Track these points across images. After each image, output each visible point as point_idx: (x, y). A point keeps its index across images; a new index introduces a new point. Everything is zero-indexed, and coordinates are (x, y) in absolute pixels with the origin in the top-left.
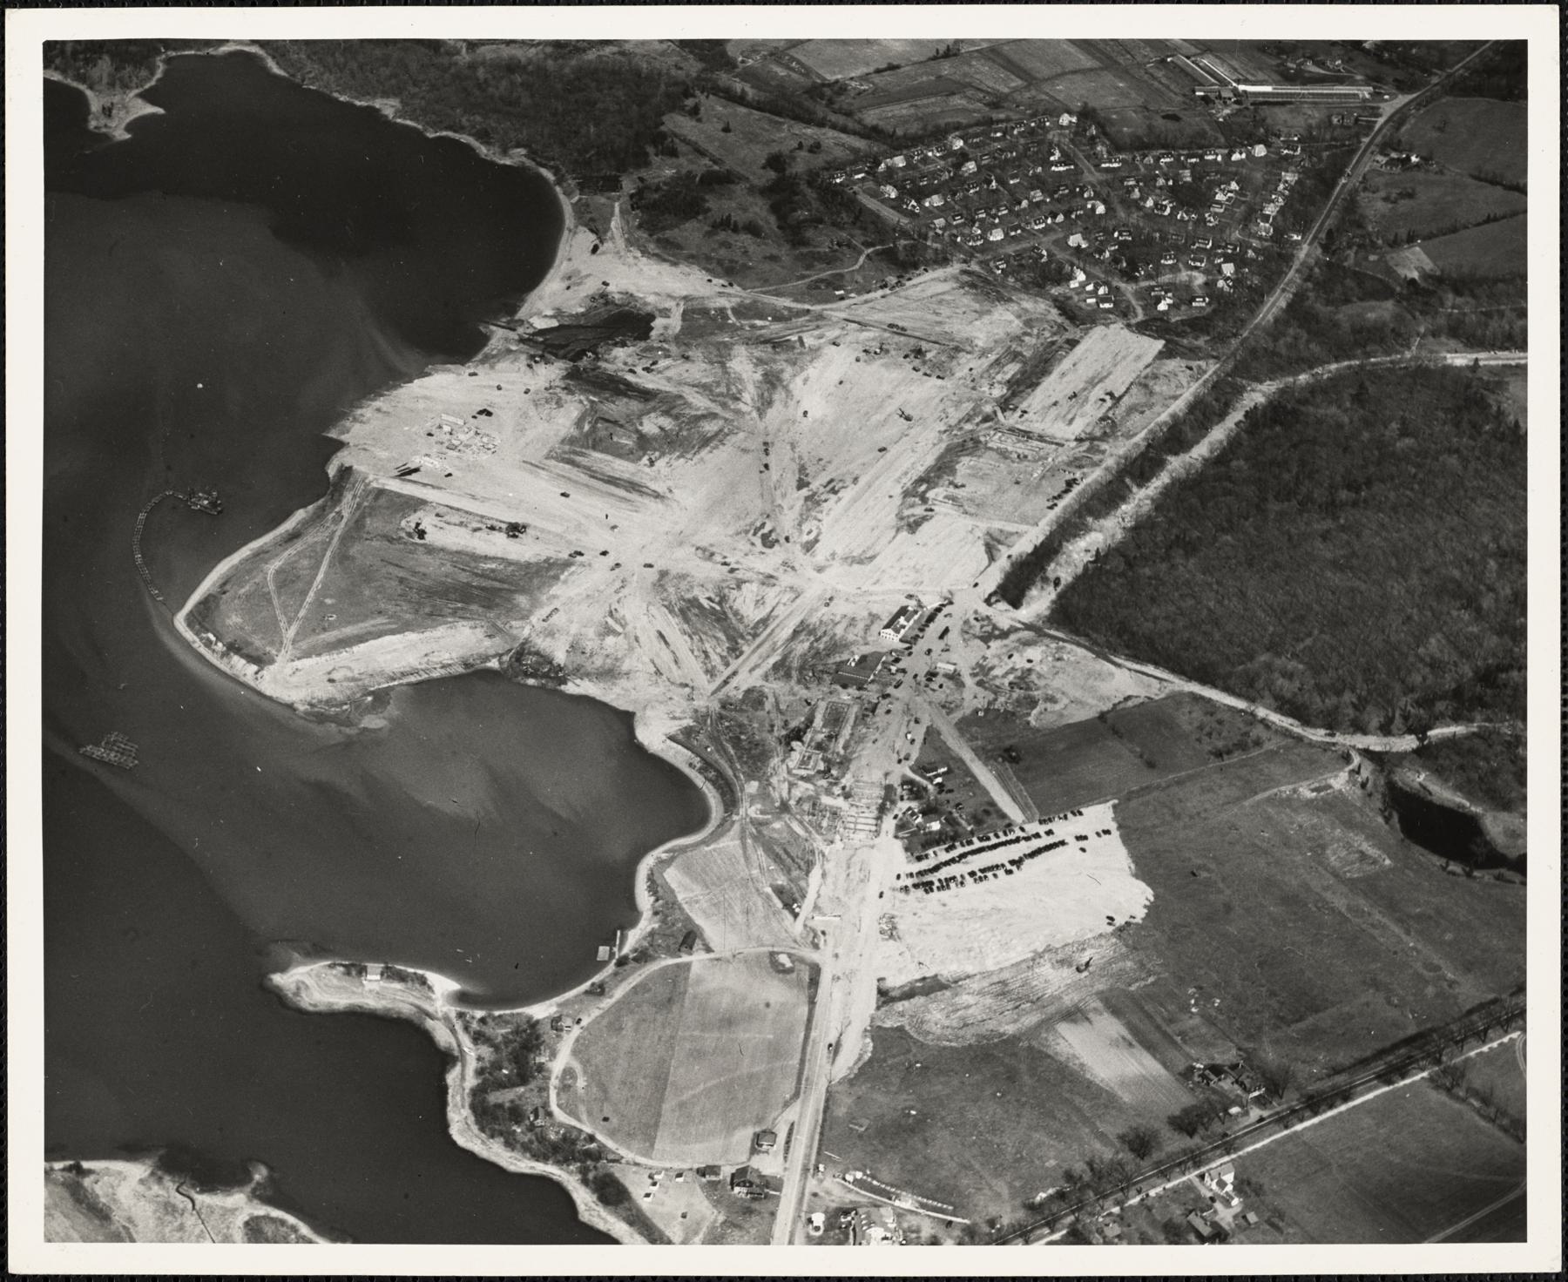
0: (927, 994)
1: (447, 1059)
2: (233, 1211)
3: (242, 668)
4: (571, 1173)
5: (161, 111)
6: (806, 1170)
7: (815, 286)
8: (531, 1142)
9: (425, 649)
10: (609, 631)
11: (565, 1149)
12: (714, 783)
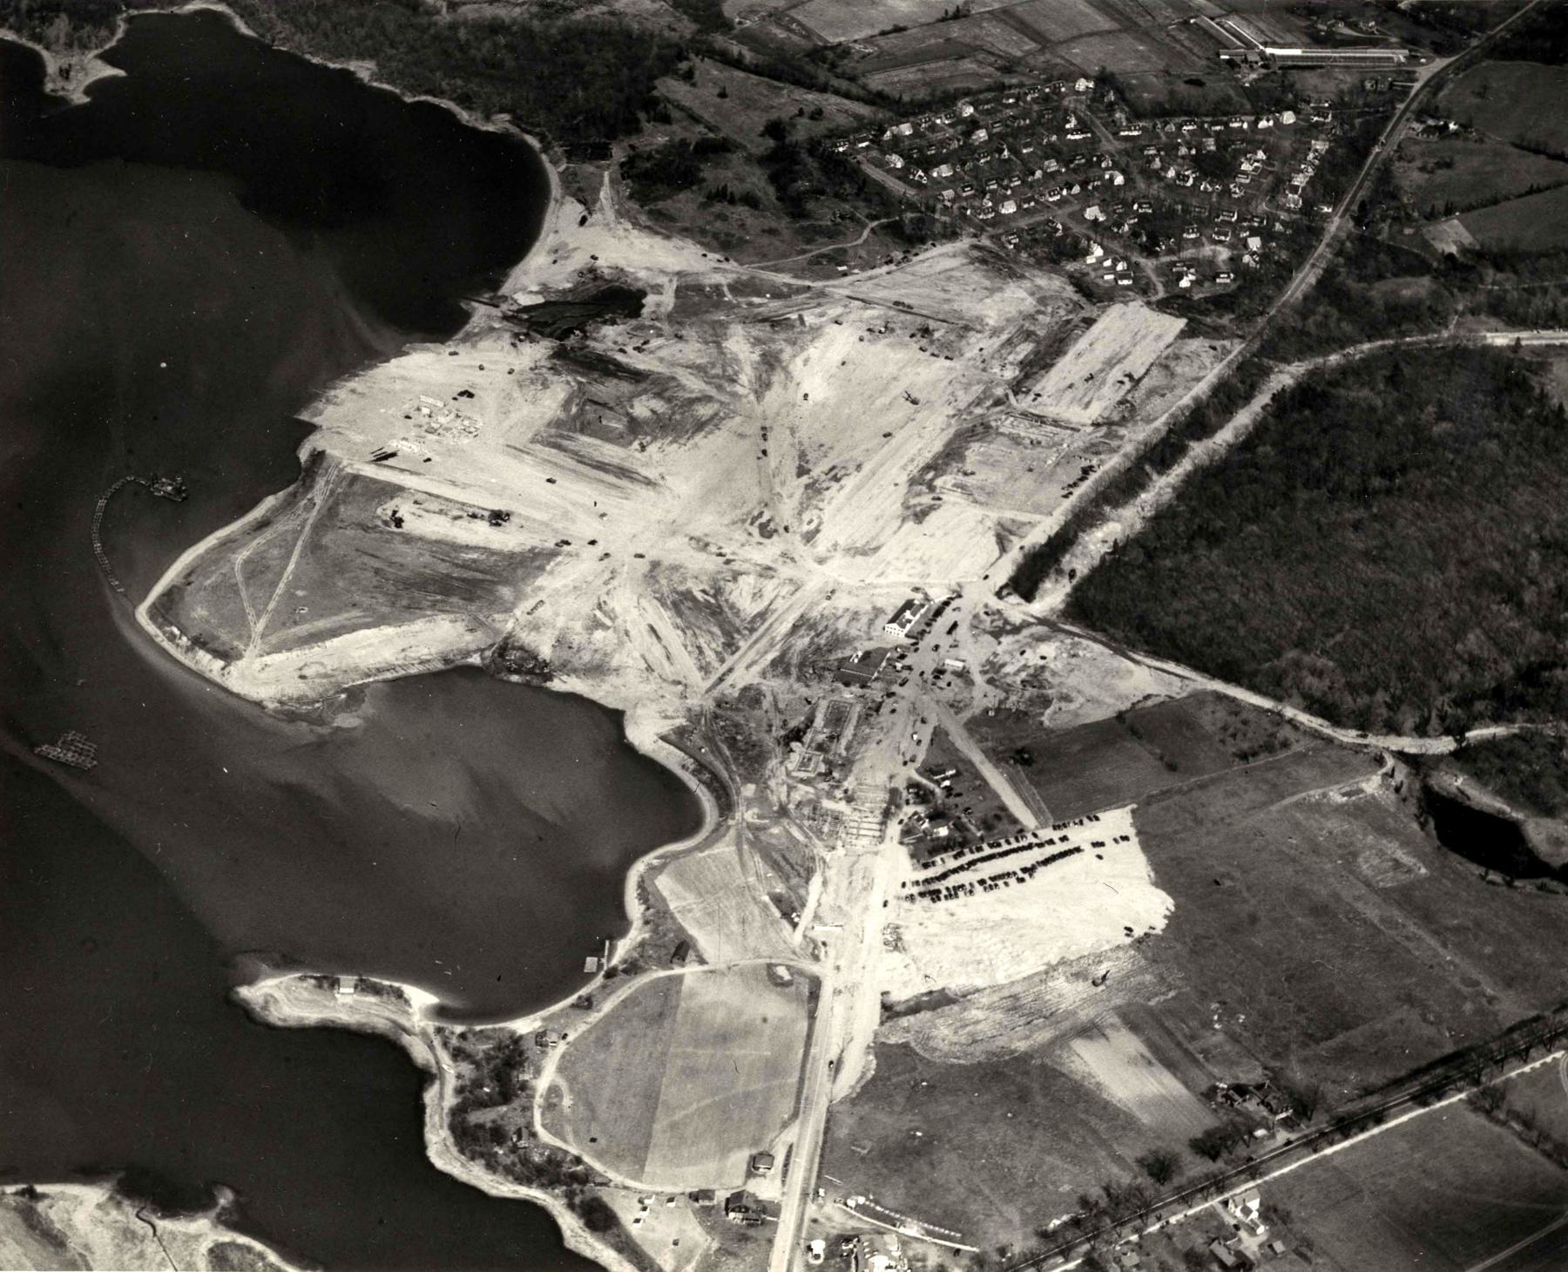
2: (197, 1237)
4: (556, 1197)
5: (121, 73)
6: (805, 1194)
9: (402, 644)
11: (551, 1172)
12: (708, 785)
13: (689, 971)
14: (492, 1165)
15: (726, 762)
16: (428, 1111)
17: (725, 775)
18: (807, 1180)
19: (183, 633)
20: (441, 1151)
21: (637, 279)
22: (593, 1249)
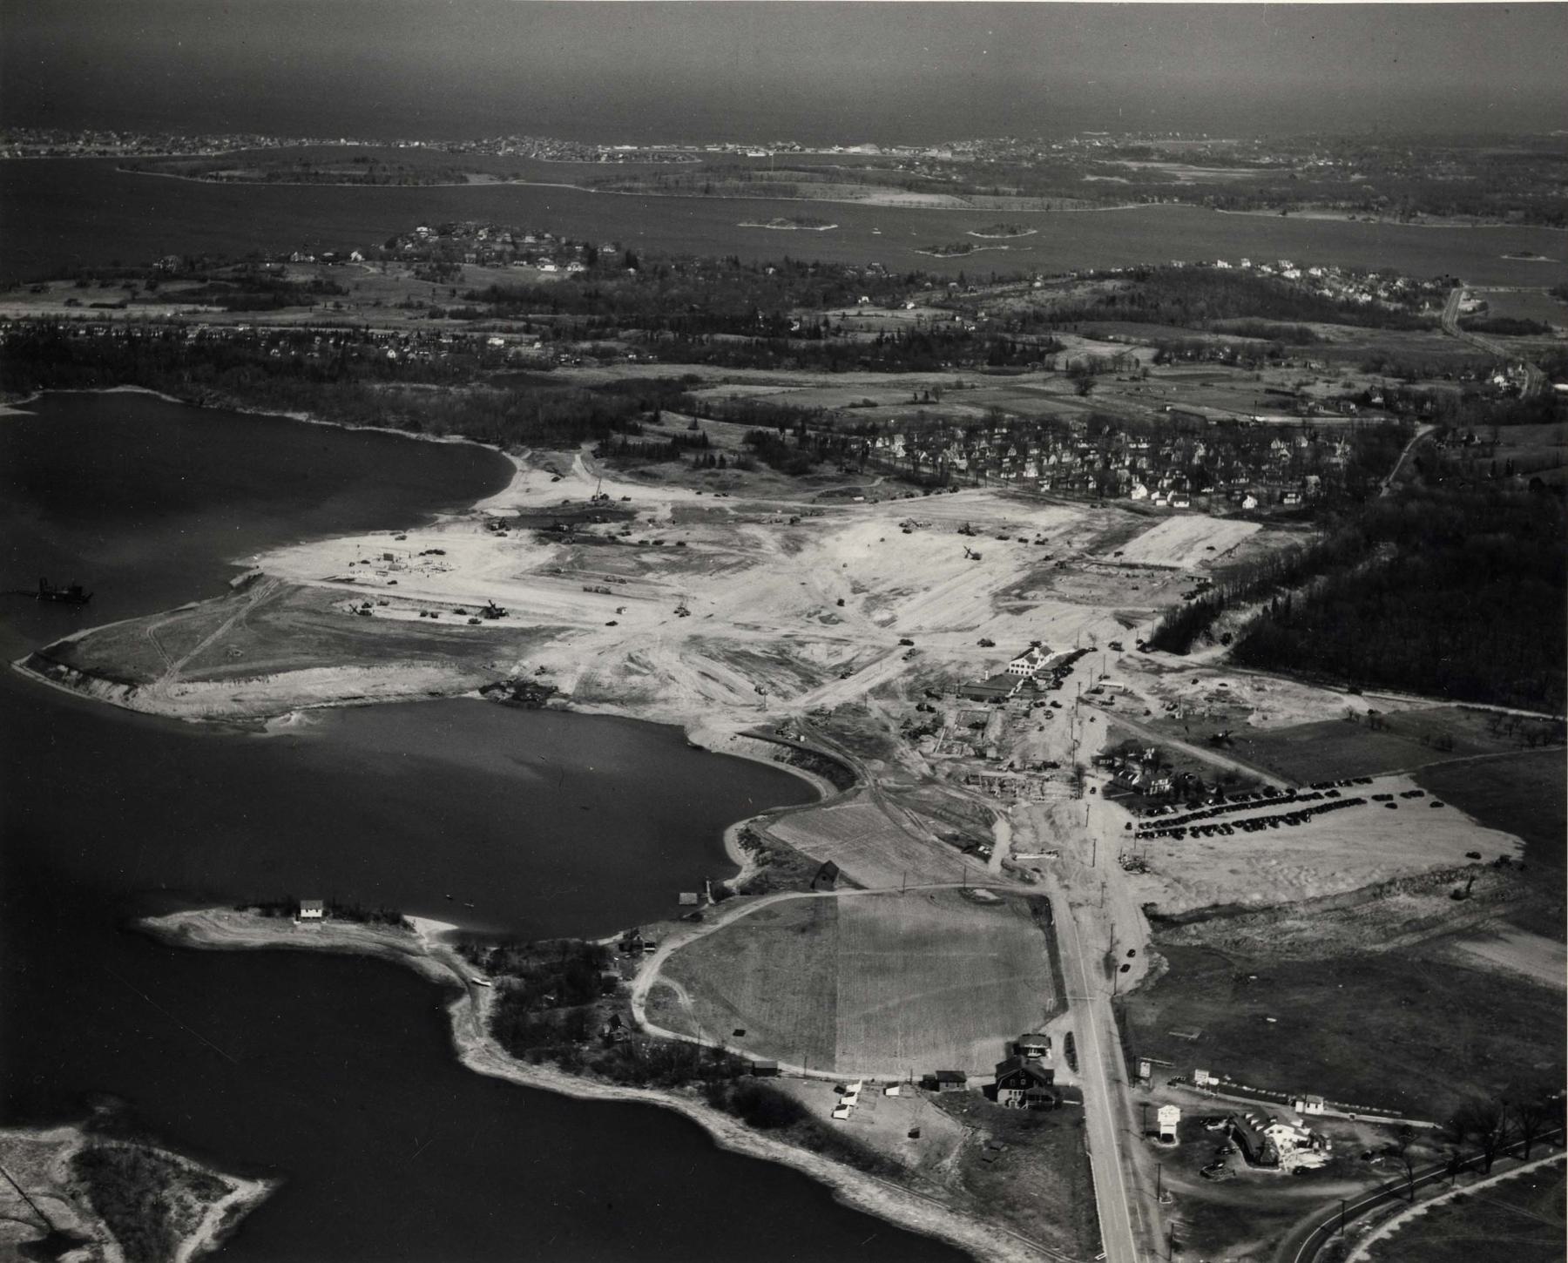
0: (1200, 277)
1: (450, 991)
2: (54, 1147)
3: (115, 694)
4: (690, 1097)
5: (154, 922)
6: (1115, 1081)
7: (822, 495)
8: (609, 1060)
9: (371, 681)
10: (630, 672)
11: (675, 1065)
12: (816, 770)
13: (844, 896)
14: (570, 1066)
15: (838, 750)
16: (455, 1022)
17: (839, 756)
18: (1111, 1066)
19: (71, 668)
20: (479, 1053)
21: (878, 1185)
22: (770, 1149)
